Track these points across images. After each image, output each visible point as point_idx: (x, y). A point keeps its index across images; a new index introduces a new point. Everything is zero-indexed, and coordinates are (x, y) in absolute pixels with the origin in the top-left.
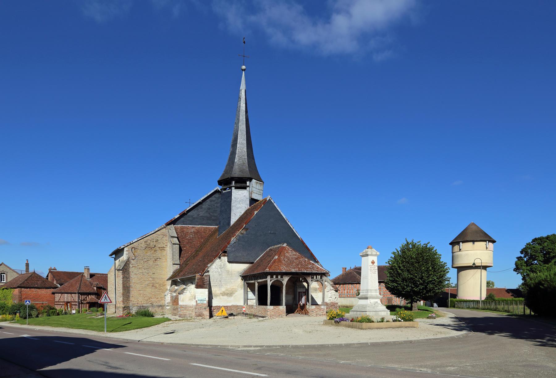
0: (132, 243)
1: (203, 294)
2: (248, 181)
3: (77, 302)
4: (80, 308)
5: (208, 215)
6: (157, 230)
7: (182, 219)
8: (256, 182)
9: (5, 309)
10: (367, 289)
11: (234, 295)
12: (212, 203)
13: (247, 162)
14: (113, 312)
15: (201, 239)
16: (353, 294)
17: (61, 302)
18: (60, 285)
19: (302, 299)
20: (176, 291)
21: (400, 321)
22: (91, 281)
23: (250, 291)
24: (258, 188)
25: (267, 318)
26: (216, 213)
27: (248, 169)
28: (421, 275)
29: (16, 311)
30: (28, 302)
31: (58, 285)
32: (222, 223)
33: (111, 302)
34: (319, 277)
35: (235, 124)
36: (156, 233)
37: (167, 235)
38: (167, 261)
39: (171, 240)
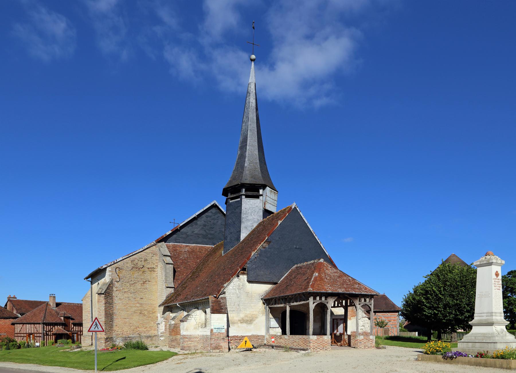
0: (115, 262)
2: (261, 189)
3: (41, 333)
4: (45, 340)
5: (204, 233)
6: (146, 247)
7: (175, 236)
8: (270, 190)
10: (490, 312)
11: (255, 322)
12: (209, 219)
13: (259, 166)
14: (89, 345)
15: (197, 260)
17: (22, 333)
19: (339, 328)
20: (175, 319)
22: (57, 310)
23: (272, 317)
25: (309, 351)
26: (213, 231)
31: (18, 315)
33: (89, 331)
36: (145, 251)
38: (157, 284)
39: (164, 259)
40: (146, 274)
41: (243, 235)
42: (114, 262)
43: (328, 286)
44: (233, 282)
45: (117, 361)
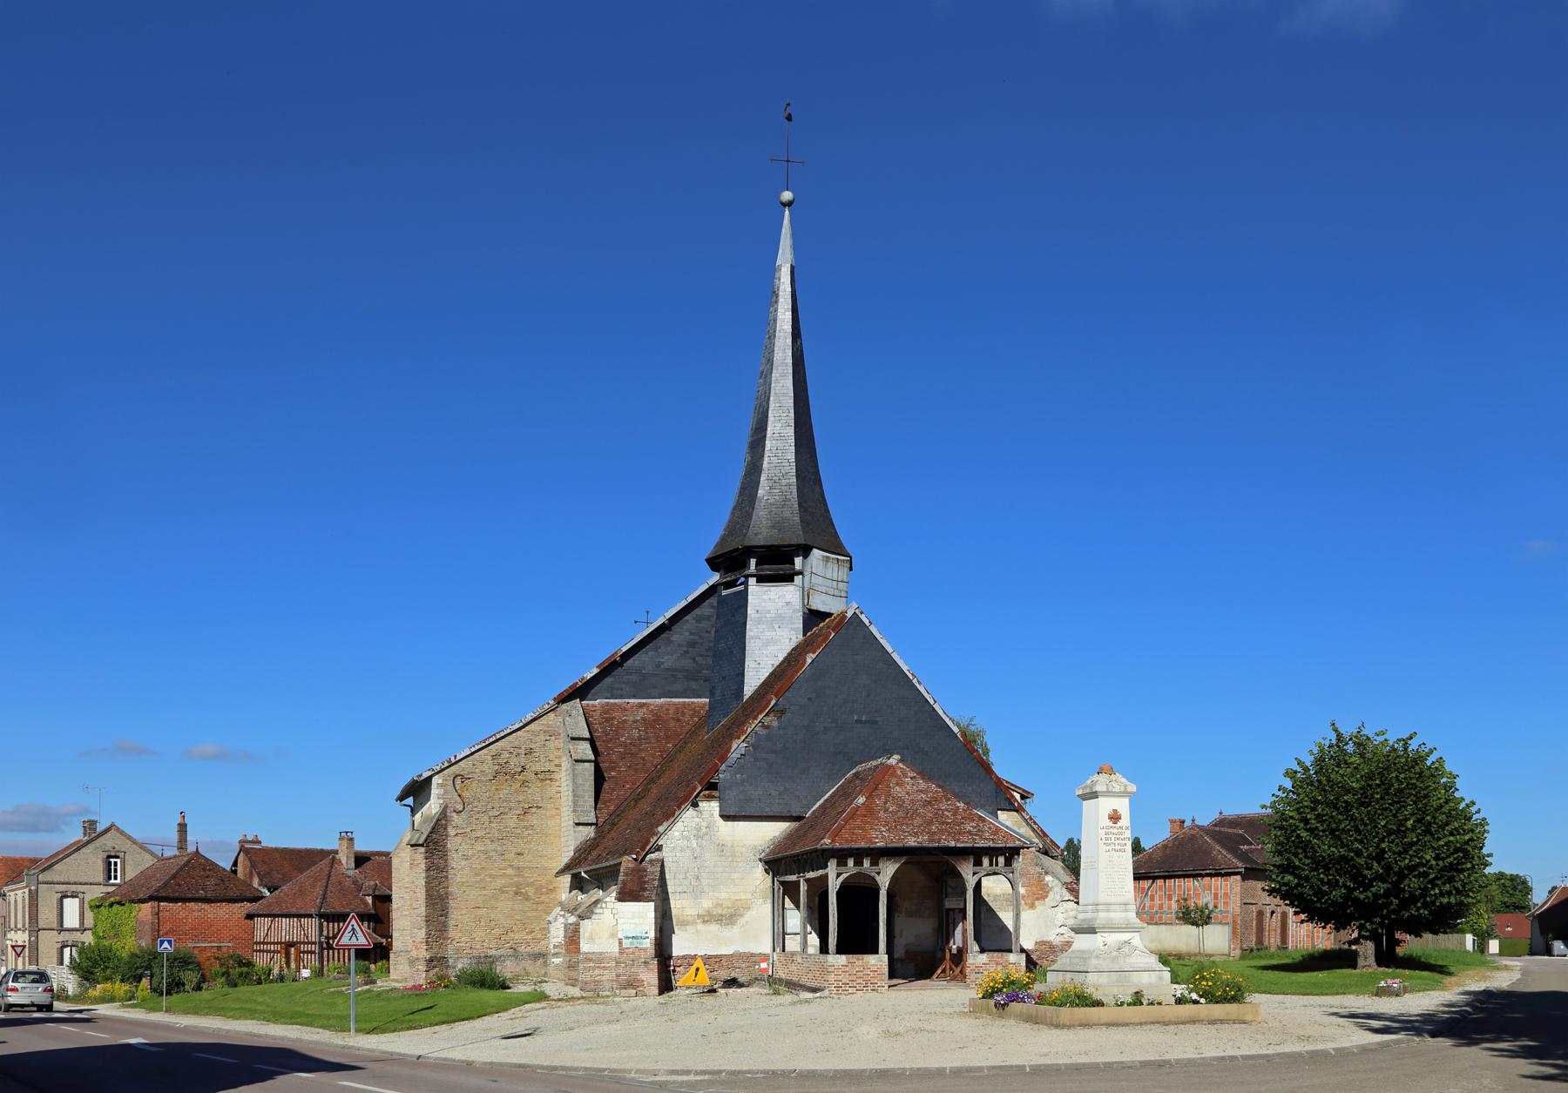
0: (453, 761)
1: (638, 918)
3: (315, 943)
6: (529, 718)
7: (608, 680)
8: (823, 556)
9: (111, 965)
10: (1096, 902)
11: (742, 921)
13: (795, 494)
18: (269, 890)
21: (1196, 1002)
24: (829, 576)
25: (826, 993)
27: (798, 518)
28: (1377, 847)
29: (140, 971)
30: (166, 945)
32: (718, 692)
34: (1001, 860)
35: (761, 378)
37: (559, 734)
42: (450, 761)
43: (881, 832)
44: (682, 819)
45: (413, 1013)
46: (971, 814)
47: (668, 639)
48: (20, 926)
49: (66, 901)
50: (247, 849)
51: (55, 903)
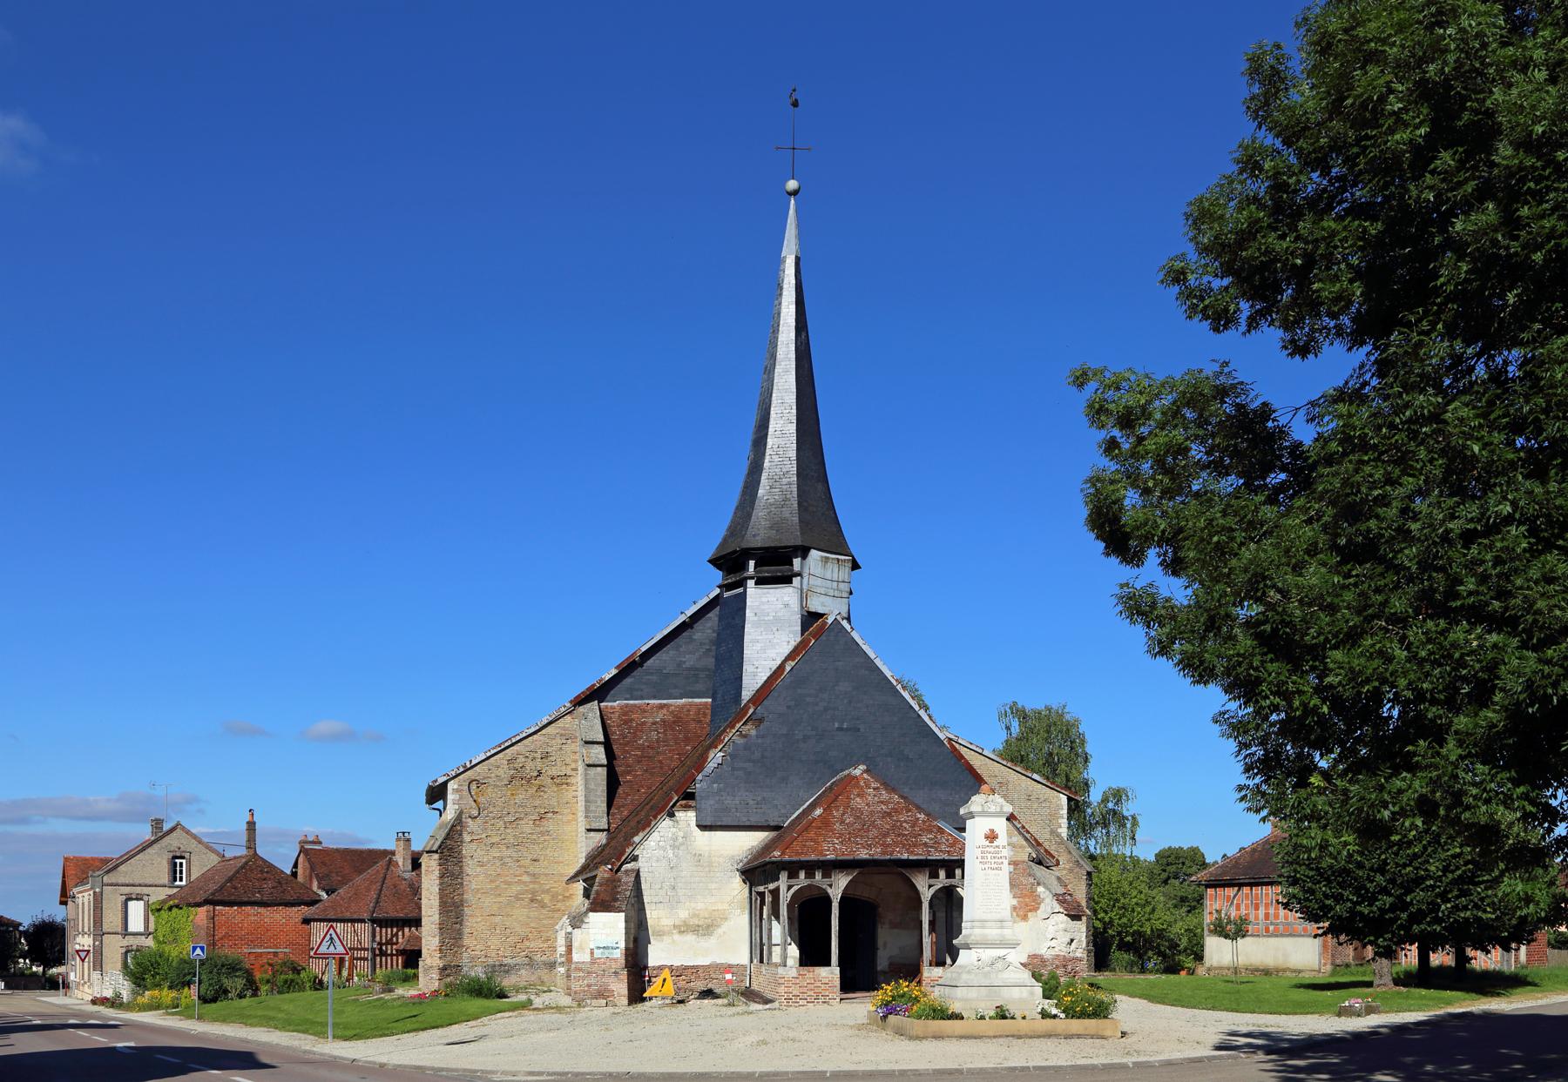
0: (469, 766)
1: (608, 930)
3: (367, 949)
6: (545, 721)
7: (628, 681)
8: (822, 557)
11: (720, 931)
13: (795, 494)
16: (1288, 924)
25: (776, 1004)
36: (543, 732)
37: (576, 738)
40: (545, 792)
41: (746, 694)
42: (465, 766)
46: (930, 825)
47: (690, 637)
48: (86, 930)
49: (131, 904)
50: (307, 850)
51: (119, 906)
